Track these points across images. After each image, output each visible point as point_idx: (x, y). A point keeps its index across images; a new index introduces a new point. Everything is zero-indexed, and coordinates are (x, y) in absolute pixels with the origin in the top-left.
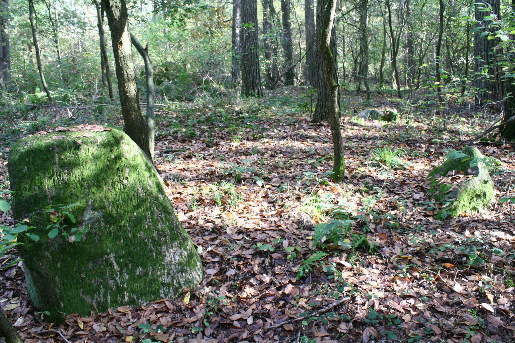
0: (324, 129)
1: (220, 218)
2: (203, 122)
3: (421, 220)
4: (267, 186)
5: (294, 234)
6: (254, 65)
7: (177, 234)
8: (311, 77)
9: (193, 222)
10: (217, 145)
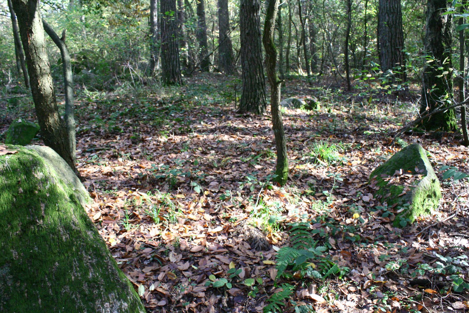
0: (251, 120)
1: (159, 239)
2: (126, 115)
3: (379, 229)
4: (206, 193)
5: (248, 257)
6: (174, 54)
7: (114, 282)
8: (226, 64)
9: (129, 248)
10: (143, 141)
